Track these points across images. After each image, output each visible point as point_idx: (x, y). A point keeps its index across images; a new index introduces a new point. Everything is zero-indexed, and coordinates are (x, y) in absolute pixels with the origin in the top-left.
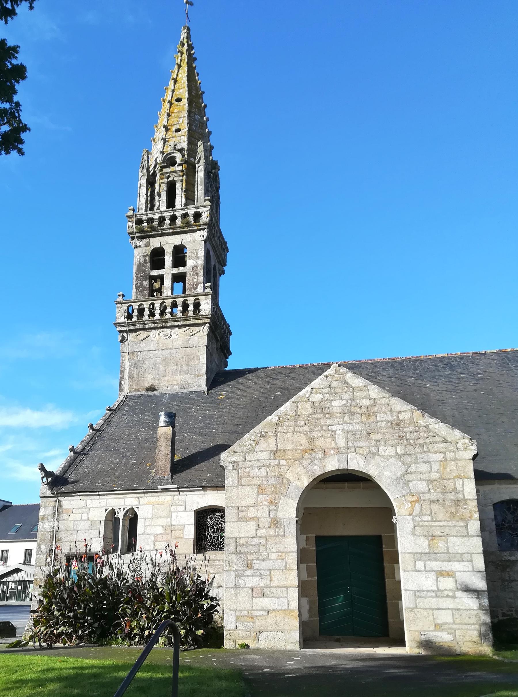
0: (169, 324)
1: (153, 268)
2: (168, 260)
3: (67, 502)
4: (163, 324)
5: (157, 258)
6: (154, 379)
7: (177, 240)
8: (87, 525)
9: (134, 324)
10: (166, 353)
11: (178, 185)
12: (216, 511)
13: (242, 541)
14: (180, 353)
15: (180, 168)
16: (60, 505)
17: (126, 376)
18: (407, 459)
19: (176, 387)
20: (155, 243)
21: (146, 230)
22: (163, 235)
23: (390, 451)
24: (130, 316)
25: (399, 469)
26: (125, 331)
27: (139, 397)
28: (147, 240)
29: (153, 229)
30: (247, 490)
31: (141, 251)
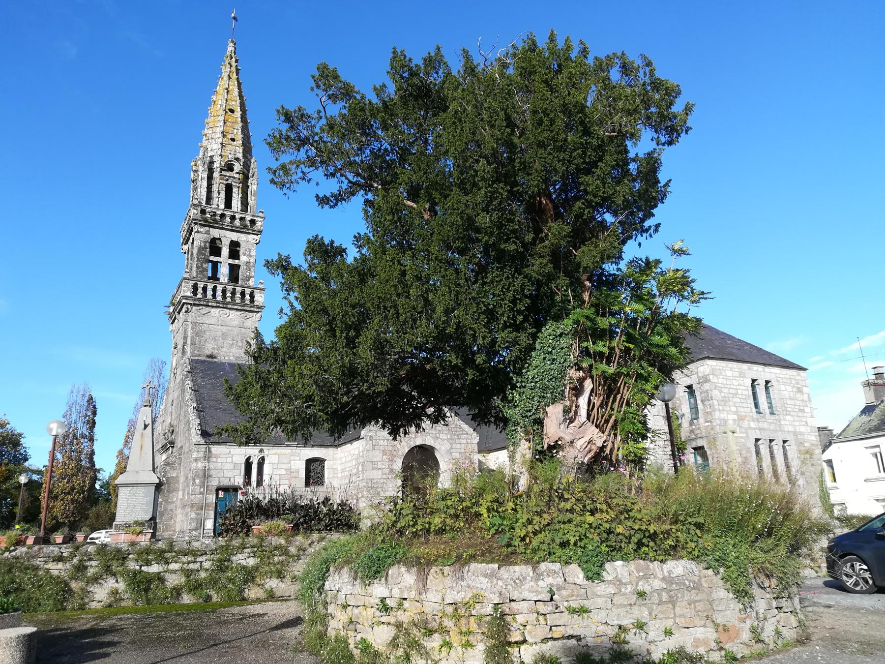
0: (230, 306)
1: (212, 254)
2: (225, 251)
3: (215, 449)
4: (223, 305)
5: (214, 247)
6: (214, 349)
7: (234, 236)
8: (232, 466)
9: (199, 300)
10: (224, 329)
11: (235, 190)
12: (321, 461)
13: (375, 481)
14: (236, 331)
15: (237, 176)
16: (210, 451)
17: (189, 342)
18: (452, 441)
19: (232, 358)
20: (215, 233)
21: (210, 221)
22: (222, 228)
23: (444, 436)
24: (195, 292)
25: (448, 446)
26: (191, 304)
27: (203, 362)
28: (207, 228)
29: (215, 221)
30: (377, 453)
31: (200, 237)
